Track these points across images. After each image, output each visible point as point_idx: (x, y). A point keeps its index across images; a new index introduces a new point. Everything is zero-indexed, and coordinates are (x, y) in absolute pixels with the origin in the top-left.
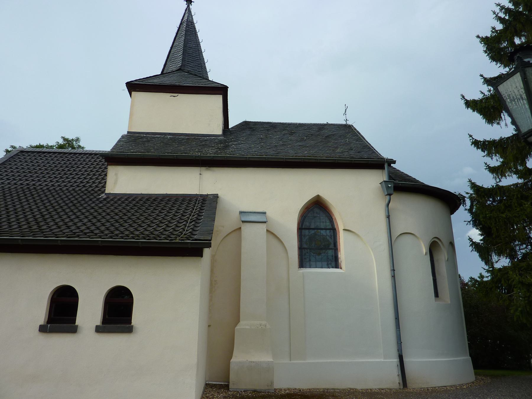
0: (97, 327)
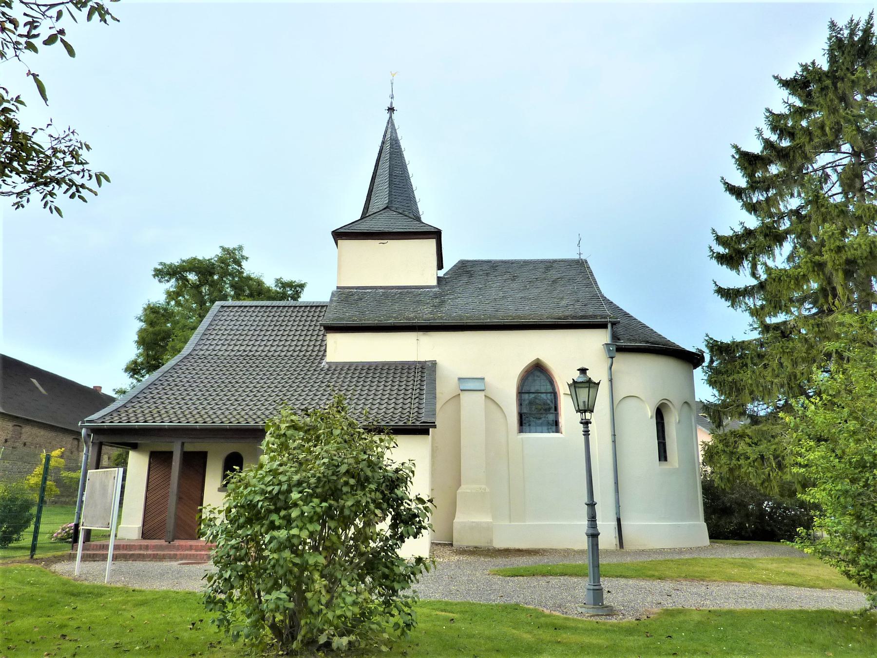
0: (219, 488)
